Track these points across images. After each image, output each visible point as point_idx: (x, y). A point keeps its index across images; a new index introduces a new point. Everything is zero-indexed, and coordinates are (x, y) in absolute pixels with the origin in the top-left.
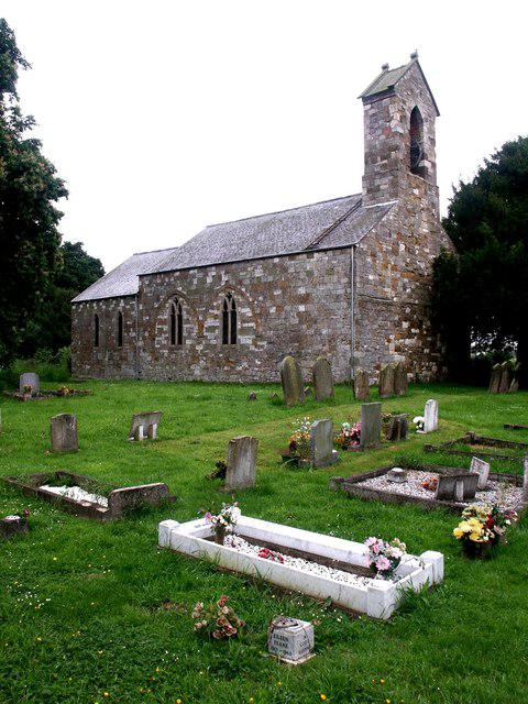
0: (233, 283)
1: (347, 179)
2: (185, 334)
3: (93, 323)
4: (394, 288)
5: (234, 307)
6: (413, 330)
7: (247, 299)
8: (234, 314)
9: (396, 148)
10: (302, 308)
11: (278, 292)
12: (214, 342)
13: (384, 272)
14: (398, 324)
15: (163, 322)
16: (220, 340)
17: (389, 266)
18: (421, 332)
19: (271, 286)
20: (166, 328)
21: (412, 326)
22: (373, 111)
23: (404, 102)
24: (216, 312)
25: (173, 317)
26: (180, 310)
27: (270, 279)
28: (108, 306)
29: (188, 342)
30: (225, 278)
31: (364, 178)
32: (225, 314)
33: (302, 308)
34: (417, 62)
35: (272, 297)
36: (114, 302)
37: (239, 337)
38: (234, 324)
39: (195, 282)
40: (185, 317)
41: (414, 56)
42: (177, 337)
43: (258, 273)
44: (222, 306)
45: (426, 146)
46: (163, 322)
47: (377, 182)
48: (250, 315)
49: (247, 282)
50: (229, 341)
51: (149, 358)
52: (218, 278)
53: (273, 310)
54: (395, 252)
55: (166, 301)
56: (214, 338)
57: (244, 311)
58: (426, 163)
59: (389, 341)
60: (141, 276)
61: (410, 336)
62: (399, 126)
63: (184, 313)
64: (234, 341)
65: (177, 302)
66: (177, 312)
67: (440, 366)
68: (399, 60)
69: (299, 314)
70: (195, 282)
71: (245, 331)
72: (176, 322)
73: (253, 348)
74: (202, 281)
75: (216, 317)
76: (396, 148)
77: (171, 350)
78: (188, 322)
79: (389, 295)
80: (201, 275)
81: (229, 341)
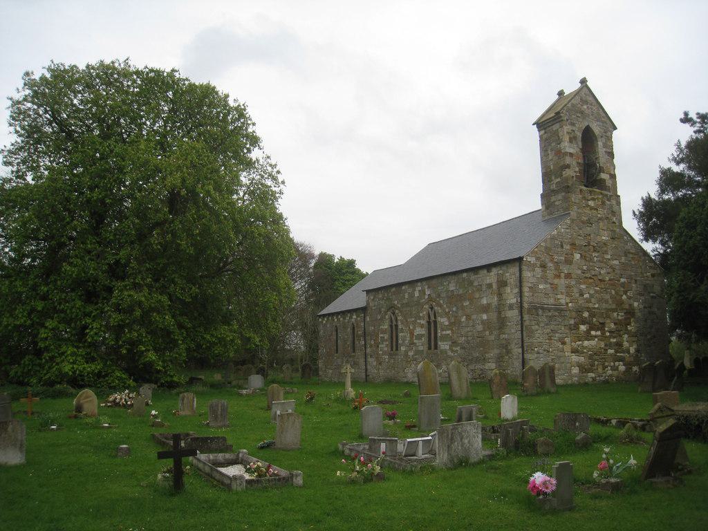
0: (434, 296)
1: (528, 198)
2: (400, 342)
3: (334, 333)
4: (568, 295)
5: (435, 317)
6: (593, 333)
7: (444, 310)
8: (435, 322)
9: (568, 166)
10: (485, 317)
11: (466, 303)
12: (421, 348)
13: (556, 281)
14: (576, 327)
15: (384, 332)
16: (426, 346)
17: (563, 275)
18: (603, 333)
19: (461, 298)
20: (386, 336)
21: (591, 328)
22: (545, 136)
23: (573, 124)
24: (423, 322)
25: (391, 326)
26: (397, 320)
27: (461, 292)
28: (344, 319)
29: (403, 349)
30: (428, 292)
31: (543, 196)
32: (429, 323)
33: (485, 317)
34: (587, 86)
35: (463, 308)
36: (349, 315)
37: (439, 343)
38: (436, 333)
39: (407, 296)
40: (400, 327)
41: (583, 81)
42: (394, 345)
43: (452, 287)
44: (426, 317)
45: (602, 159)
46: (384, 332)
47: (553, 199)
48: (447, 323)
49: (444, 295)
50: (433, 347)
51: (375, 363)
52: (422, 292)
53: (463, 319)
54: (569, 262)
55: (386, 313)
56: (421, 345)
57: (442, 320)
58: (603, 176)
59: (564, 343)
60: (368, 292)
61: (588, 336)
62: (571, 148)
63: (399, 323)
64: (436, 347)
65: (394, 313)
66: (433, 318)
67: (628, 365)
68: (571, 87)
69: (483, 322)
70: (407, 296)
71: (445, 338)
72: (394, 329)
73: (450, 353)
74: (412, 295)
75: (422, 326)
76: (568, 166)
77: (390, 355)
78: (402, 331)
79: (563, 301)
80: (410, 290)
81: (433, 347)
